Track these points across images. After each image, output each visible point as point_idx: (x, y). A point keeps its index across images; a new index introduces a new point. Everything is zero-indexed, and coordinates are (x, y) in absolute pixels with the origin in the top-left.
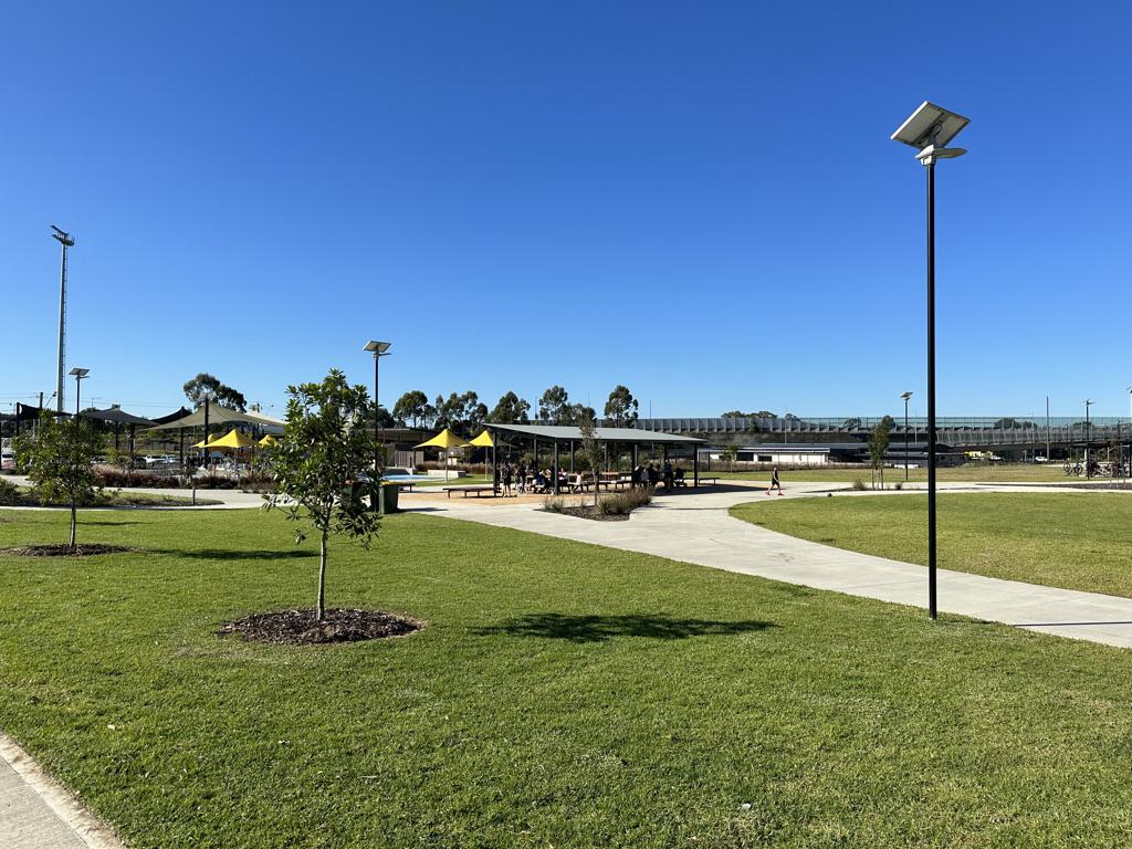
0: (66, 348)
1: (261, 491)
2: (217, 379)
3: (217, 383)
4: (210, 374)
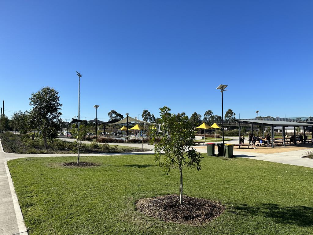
1: (154, 144)
2: (116, 111)
3: (116, 112)
4: (114, 110)
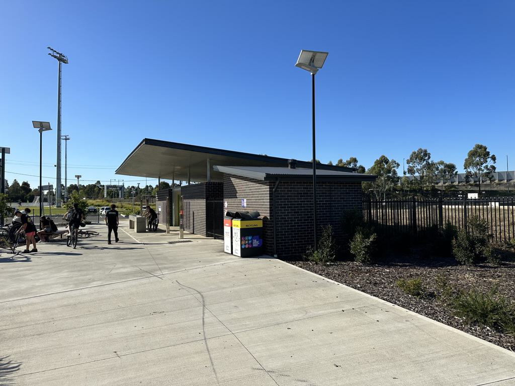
0: (62, 88)
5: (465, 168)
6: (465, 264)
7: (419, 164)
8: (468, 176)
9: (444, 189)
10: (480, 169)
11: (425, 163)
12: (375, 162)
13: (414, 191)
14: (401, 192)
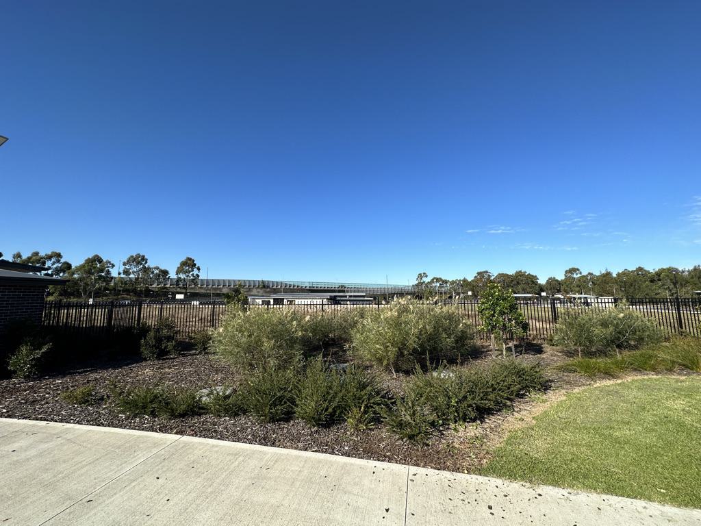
5: (177, 274)
6: (149, 360)
7: (135, 267)
8: (179, 280)
9: (157, 290)
10: (187, 276)
11: (142, 266)
12: (86, 260)
13: (127, 291)
14: (113, 292)
